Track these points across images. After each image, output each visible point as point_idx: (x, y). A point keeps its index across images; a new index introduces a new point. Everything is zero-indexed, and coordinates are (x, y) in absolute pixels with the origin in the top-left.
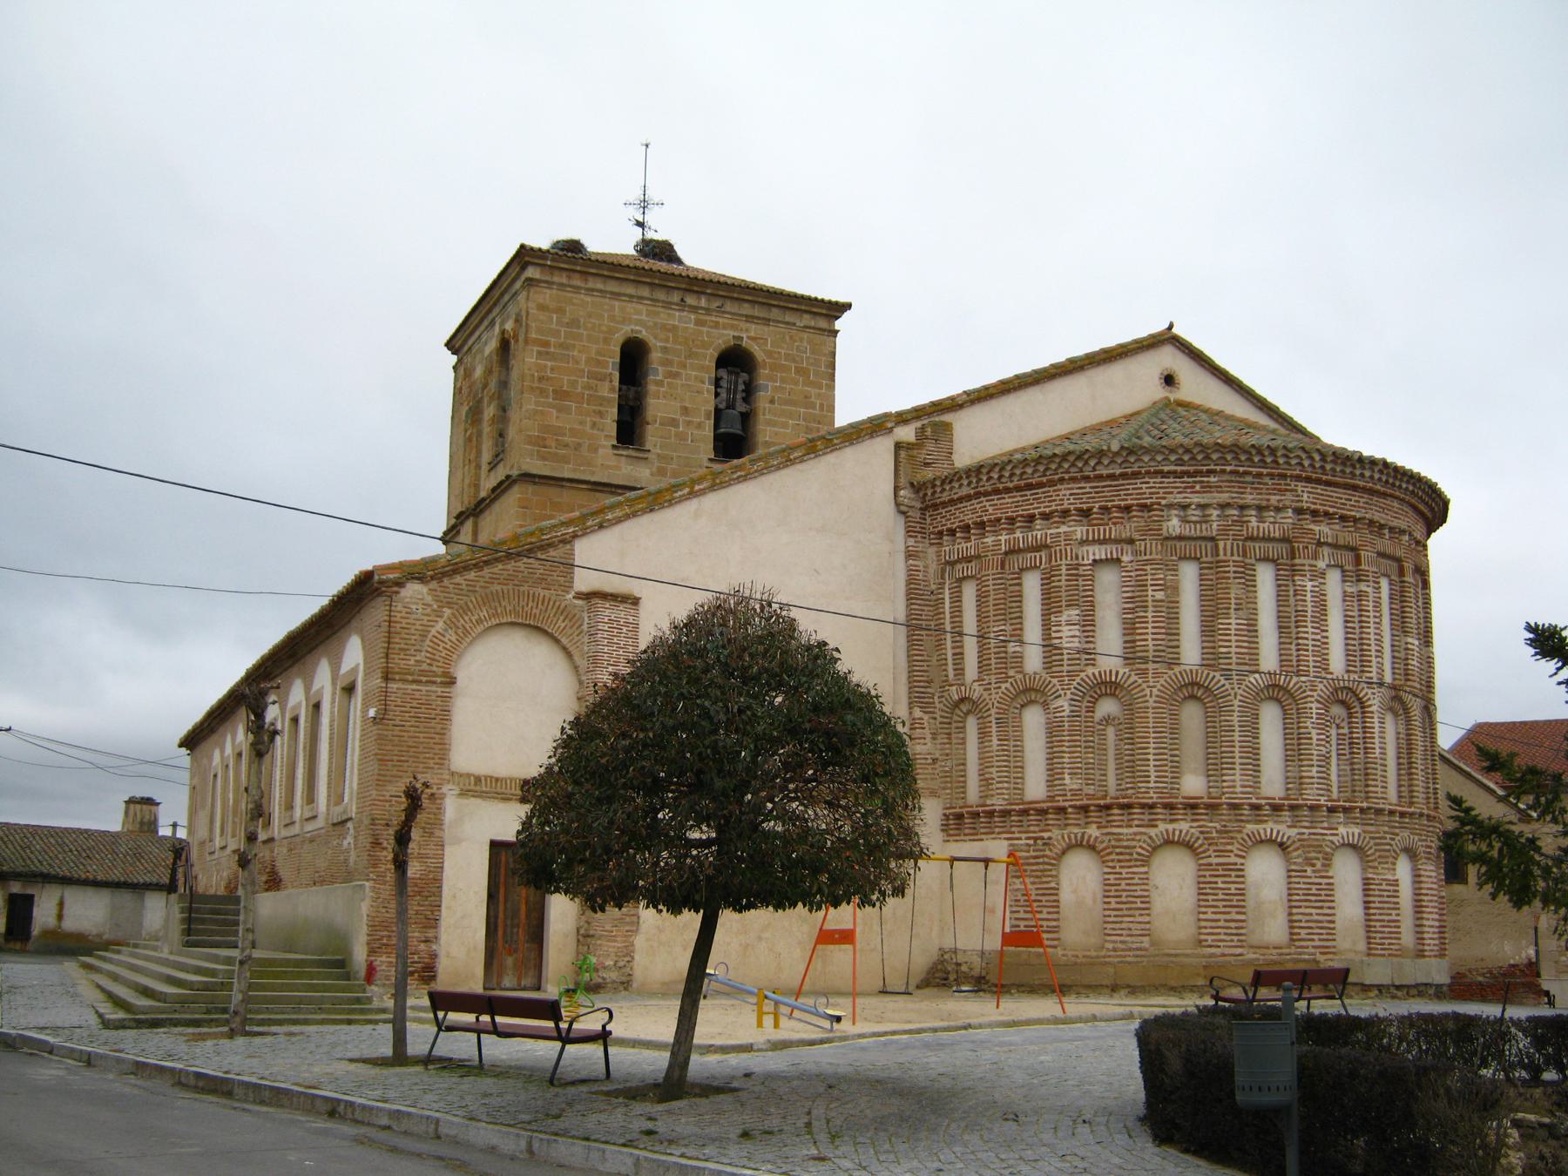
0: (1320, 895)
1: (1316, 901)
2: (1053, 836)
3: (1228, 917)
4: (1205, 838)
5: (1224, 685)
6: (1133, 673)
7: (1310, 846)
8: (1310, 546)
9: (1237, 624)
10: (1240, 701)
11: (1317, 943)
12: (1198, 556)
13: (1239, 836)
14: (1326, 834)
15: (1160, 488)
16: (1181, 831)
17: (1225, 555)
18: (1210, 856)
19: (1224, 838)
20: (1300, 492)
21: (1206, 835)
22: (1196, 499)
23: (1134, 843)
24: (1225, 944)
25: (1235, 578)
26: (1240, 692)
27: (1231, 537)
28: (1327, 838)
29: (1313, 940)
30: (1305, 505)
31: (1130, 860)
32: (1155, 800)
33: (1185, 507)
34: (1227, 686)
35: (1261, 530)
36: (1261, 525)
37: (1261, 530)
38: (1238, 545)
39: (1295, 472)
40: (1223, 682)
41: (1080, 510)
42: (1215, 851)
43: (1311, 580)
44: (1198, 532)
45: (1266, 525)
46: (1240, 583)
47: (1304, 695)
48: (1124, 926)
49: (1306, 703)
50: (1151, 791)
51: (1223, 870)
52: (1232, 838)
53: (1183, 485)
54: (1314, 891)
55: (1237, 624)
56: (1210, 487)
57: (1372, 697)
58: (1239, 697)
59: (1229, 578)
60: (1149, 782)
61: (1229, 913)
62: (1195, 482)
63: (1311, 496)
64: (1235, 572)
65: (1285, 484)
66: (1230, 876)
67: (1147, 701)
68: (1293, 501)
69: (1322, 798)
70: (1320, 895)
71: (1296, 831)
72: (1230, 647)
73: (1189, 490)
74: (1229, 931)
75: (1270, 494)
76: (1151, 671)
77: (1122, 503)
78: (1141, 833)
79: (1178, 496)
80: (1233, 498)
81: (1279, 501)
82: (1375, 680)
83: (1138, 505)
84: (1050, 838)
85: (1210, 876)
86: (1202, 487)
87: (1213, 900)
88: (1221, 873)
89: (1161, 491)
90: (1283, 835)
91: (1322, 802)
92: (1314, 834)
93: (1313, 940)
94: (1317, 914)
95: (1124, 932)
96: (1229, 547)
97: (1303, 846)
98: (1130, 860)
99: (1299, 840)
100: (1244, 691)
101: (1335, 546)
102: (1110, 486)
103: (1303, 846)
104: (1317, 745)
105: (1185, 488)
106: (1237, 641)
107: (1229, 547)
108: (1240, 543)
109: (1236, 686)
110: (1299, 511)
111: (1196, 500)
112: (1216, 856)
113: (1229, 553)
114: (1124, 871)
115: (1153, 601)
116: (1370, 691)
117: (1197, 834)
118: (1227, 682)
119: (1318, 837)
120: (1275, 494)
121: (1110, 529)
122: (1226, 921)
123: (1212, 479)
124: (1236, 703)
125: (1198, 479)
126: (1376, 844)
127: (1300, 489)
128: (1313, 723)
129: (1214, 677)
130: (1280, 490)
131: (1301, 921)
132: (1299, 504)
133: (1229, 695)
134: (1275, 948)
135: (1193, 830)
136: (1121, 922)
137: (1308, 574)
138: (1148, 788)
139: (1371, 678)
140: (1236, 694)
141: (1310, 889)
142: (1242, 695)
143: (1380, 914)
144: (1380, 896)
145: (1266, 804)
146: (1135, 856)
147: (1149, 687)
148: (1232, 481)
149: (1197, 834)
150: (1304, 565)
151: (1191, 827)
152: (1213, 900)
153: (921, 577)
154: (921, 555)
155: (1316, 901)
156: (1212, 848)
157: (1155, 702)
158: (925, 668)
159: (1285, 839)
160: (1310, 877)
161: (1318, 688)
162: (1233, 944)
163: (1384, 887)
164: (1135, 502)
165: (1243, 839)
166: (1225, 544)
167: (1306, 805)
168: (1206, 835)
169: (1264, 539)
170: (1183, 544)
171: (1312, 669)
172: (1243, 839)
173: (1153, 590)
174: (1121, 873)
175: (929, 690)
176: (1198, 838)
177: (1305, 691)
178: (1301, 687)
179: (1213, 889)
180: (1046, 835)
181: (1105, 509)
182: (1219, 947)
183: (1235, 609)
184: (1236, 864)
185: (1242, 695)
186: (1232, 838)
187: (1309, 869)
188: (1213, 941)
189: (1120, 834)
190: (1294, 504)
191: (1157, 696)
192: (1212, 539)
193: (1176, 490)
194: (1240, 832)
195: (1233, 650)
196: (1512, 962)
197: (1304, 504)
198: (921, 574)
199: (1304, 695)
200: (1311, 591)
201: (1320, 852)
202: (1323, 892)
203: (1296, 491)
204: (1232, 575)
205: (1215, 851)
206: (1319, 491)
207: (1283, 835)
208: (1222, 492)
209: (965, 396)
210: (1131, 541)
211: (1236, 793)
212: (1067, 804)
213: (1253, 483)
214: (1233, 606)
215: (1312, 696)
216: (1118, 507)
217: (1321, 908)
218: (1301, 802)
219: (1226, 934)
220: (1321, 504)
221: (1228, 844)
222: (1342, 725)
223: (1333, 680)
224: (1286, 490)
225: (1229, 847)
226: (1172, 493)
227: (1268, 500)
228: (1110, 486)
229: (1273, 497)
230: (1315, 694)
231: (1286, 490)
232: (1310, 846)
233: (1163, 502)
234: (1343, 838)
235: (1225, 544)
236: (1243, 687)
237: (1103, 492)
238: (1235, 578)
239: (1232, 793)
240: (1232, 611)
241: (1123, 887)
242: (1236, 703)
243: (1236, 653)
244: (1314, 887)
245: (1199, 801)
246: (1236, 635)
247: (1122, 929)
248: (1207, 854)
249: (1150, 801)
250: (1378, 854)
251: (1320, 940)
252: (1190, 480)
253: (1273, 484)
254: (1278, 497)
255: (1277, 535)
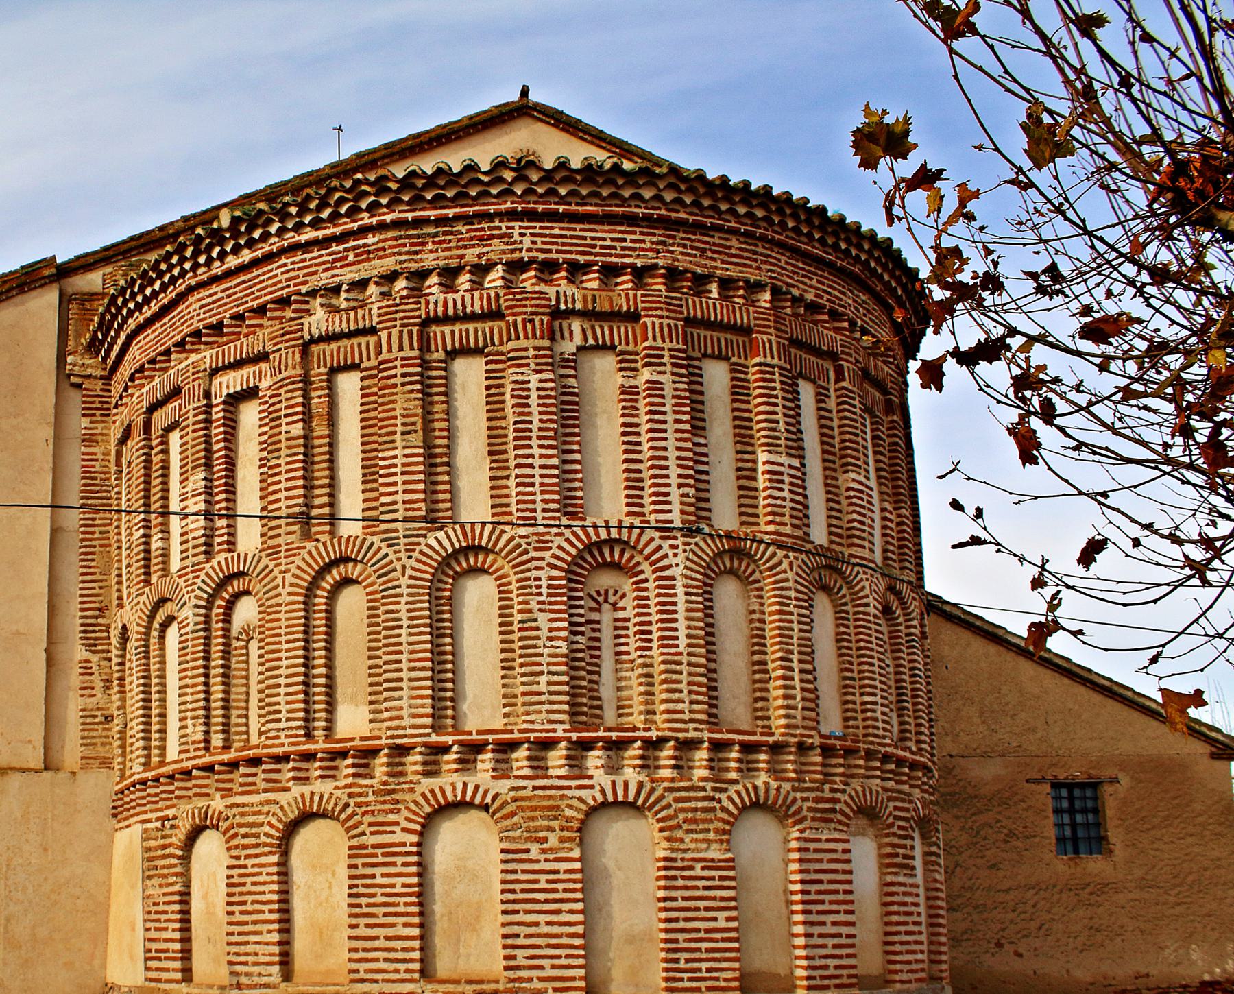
0: (555, 891)
1: (547, 901)
2: (179, 815)
3: (390, 932)
4: (359, 805)
5: (386, 555)
6: (263, 554)
7: (534, 809)
8: (537, 319)
9: (406, 456)
10: (411, 577)
11: (550, 973)
12: (357, 361)
13: (408, 797)
14: (570, 788)
15: (299, 269)
16: (322, 796)
17: (390, 351)
18: (363, 834)
19: (384, 802)
20: (517, 237)
21: (359, 800)
22: (349, 275)
23: (261, 818)
24: (386, 976)
25: (403, 384)
26: (409, 563)
27: (398, 323)
28: (569, 793)
29: (541, 968)
30: (526, 256)
31: (257, 845)
32: (286, 748)
33: (336, 290)
34: (392, 557)
35: (451, 304)
36: (450, 296)
37: (451, 304)
38: (410, 333)
39: (503, 207)
40: (384, 551)
41: (210, 327)
42: (371, 824)
43: (537, 372)
44: (352, 323)
45: (458, 296)
46: (412, 392)
47: (525, 557)
48: (249, 949)
49: (529, 570)
50: (282, 734)
51: (384, 855)
52: (398, 802)
53: (330, 258)
54: (543, 885)
55: (406, 456)
56: (369, 252)
57: (670, 552)
58: (409, 572)
59: (395, 386)
60: (279, 720)
61: (393, 925)
62: (346, 250)
63: (539, 240)
64: (403, 375)
65: (490, 229)
66: (394, 864)
67: (280, 595)
68: (503, 252)
69: (560, 727)
70: (555, 891)
71: (508, 784)
72: (396, 493)
73: (339, 264)
74: (392, 955)
75: (465, 247)
76: (284, 548)
77: (255, 303)
78: (268, 802)
79: (324, 275)
80: (401, 262)
81: (479, 256)
82: (677, 524)
83: (274, 301)
84: (175, 818)
85: (364, 865)
86: (356, 255)
87: (368, 905)
88: (381, 859)
89: (301, 273)
90: (486, 792)
91: (560, 734)
92: (543, 788)
93: (541, 968)
94: (548, 923)
95: (250, 959)
96: (395, 338)
97: (522, 809)
98: (257, 845)
99: (515, 800)
100: (418, 561)
101: (584, 314)
102: (244, 282)
103: (522, 809)
104: (550, 639)
105: (335, 261)
106: (405, 482)
107: (395, 338)
108: (415, 329)
109: (403, 555)
110: (516, 267)
111: (349, 276)
112: (372, 833)
113: (395, 346)
114: (250, 862)
115: (288, 439)
116: (666, 544)
117: (345, 799)
118: (390, 551)
119: (553, 792)
120: (473, 246)
121: (242, 344)
122: (387, 938)
123: (371, 239)
124: (404, 581)
125: (352, 244)
126: (677, 800)
127: (516, 232)
128: (542, 602)
129: (372, 544)
130: (481, 239)
131: (518, 936)
132: (517, 255)
133: (394, 570)
134: (470, 982)
135: (338, 793)
136: (246, 943)
137: (532, 362)
138: (278, 730)
139: (671, 522)
140: (404, 567)
141: (537, 881)
142: (413, 569)
143: (686, 920)
144: (687, 888)
145: (455, 742)
146: (263, 839)
147: (281, 572)
148: (401, 237)
149: (345, 799)
150: (526, 349)
151: (337, 788)
152: (368, 905)
153: (98, 469)
154: (100, 438)
155: (547, 901)
156: (368, 819)
157: (289, 594)
158: (97, 591)
159: (488, 800)
160: (538, 861)
161: (554, 545)
162: (397, 976)
163: (698, 872)
164: (268, 297)
165: (415, 802)
166: (390, 334)
167: (528, 740)
168: (359, 800)
169: (456, 319)
170: (334, 346)
171: (539, 515)
172: (415, 802)
173: (288, 424)
174: (245, 867)
175: (100, 621)
176: (347, 805)
177: (526, 552)
178: (519, 545)
179: (368, 886)
180: (170, 812)
181: (239, 317)
182: (376, 981)
183: (403, 433)
184: (404, 844)
185: (413, 569)
186: (398, 802)
187: (535, 849)
188: (366, 971)
189: (244, 805)
190: (505, 257)
191: (292, 585)
192: (373, 331)
193: (320, 268)
194: (412, 790)
195: (399, 497)
196: (1207, 977)
197: (524, 254)
198: (97, 464)
199: (525, 557)
200: (538, 389)
201: (556, 818)
202: (560, 886)
203: (510, 236)
204: (399, 380)
205: (371, 824)
206: (557, 231)
207: (486, 792)
208: (386, 256)
209: (181, 224)
210: (263, 357)
211: (404, 728)
212: (190, 764)
213: (436, 235)
214: (399, 429)
215: (543, 559)
216: (251, 310)
217: (558, 912)
218: (517, 735)
219: (386, 960)
220: (558, 251)
221: (391, 811)
222: (620, 604)
223: (583, 527)
224: (492, 237)
225: (392, 817)
226: (315, 273)
227: (462, 257)
228: (244, 282)
229: (469, 251)
230: (547, 554)
231: (492, 237)
232: (534, 809)
233: (304, 289)
234: (603, 792)
235: (390, 334)
236: (415, 555)
237: (236, 293)
238: (403, 384)
239: (398, 728)
240: (398, 437)
241: (248, 888)
242: (404, 581)
243: (404, 502)
244: (543, 877)
245: (348, 745)
246: (403, 473)
247: (247, 954)
248: (359, 830)
249: (279, 750)
250: (681, 816)
251: (553, 967)
252: (341, 248)
253: (469, 231)
254: (478, 250)
255: (477, 309)
